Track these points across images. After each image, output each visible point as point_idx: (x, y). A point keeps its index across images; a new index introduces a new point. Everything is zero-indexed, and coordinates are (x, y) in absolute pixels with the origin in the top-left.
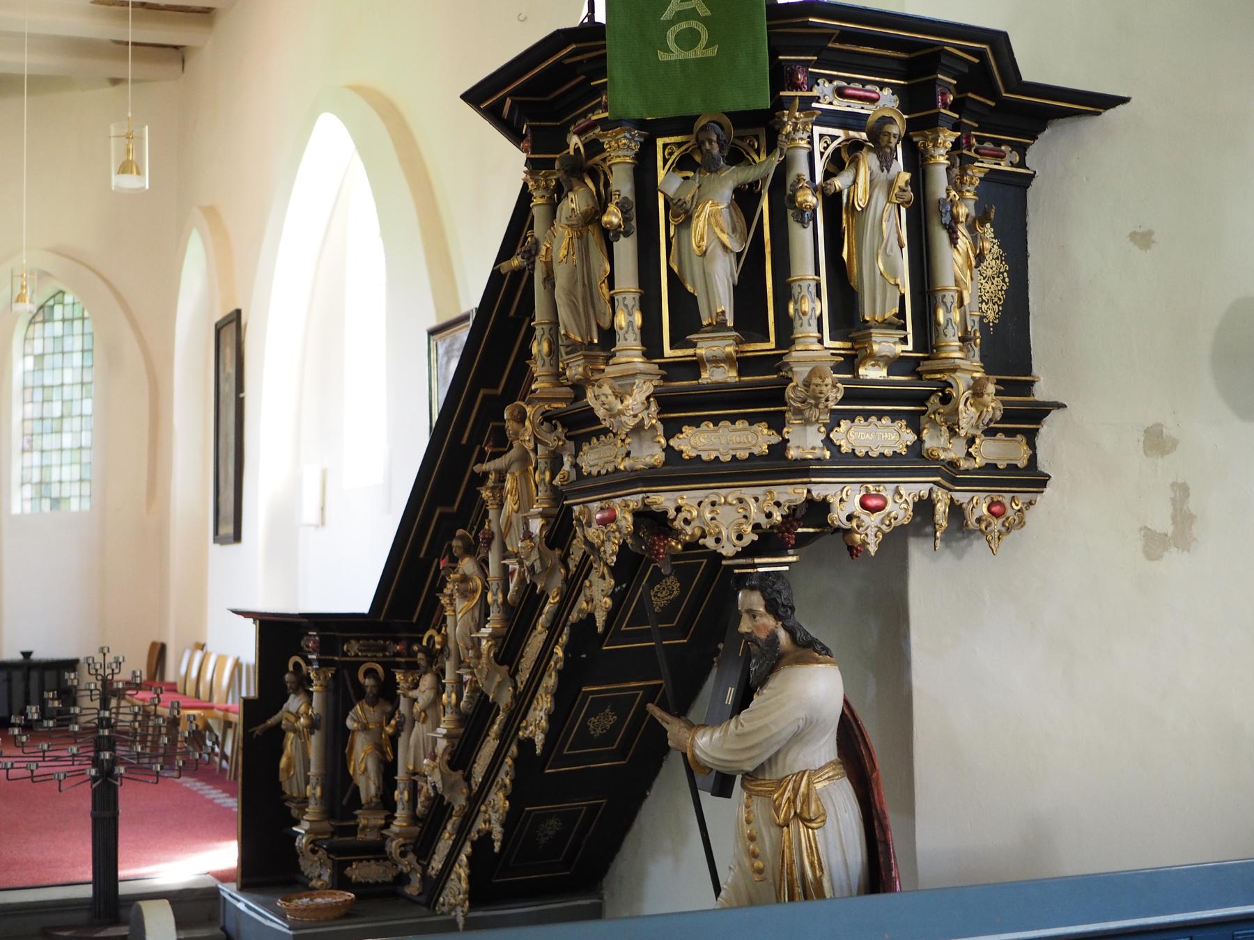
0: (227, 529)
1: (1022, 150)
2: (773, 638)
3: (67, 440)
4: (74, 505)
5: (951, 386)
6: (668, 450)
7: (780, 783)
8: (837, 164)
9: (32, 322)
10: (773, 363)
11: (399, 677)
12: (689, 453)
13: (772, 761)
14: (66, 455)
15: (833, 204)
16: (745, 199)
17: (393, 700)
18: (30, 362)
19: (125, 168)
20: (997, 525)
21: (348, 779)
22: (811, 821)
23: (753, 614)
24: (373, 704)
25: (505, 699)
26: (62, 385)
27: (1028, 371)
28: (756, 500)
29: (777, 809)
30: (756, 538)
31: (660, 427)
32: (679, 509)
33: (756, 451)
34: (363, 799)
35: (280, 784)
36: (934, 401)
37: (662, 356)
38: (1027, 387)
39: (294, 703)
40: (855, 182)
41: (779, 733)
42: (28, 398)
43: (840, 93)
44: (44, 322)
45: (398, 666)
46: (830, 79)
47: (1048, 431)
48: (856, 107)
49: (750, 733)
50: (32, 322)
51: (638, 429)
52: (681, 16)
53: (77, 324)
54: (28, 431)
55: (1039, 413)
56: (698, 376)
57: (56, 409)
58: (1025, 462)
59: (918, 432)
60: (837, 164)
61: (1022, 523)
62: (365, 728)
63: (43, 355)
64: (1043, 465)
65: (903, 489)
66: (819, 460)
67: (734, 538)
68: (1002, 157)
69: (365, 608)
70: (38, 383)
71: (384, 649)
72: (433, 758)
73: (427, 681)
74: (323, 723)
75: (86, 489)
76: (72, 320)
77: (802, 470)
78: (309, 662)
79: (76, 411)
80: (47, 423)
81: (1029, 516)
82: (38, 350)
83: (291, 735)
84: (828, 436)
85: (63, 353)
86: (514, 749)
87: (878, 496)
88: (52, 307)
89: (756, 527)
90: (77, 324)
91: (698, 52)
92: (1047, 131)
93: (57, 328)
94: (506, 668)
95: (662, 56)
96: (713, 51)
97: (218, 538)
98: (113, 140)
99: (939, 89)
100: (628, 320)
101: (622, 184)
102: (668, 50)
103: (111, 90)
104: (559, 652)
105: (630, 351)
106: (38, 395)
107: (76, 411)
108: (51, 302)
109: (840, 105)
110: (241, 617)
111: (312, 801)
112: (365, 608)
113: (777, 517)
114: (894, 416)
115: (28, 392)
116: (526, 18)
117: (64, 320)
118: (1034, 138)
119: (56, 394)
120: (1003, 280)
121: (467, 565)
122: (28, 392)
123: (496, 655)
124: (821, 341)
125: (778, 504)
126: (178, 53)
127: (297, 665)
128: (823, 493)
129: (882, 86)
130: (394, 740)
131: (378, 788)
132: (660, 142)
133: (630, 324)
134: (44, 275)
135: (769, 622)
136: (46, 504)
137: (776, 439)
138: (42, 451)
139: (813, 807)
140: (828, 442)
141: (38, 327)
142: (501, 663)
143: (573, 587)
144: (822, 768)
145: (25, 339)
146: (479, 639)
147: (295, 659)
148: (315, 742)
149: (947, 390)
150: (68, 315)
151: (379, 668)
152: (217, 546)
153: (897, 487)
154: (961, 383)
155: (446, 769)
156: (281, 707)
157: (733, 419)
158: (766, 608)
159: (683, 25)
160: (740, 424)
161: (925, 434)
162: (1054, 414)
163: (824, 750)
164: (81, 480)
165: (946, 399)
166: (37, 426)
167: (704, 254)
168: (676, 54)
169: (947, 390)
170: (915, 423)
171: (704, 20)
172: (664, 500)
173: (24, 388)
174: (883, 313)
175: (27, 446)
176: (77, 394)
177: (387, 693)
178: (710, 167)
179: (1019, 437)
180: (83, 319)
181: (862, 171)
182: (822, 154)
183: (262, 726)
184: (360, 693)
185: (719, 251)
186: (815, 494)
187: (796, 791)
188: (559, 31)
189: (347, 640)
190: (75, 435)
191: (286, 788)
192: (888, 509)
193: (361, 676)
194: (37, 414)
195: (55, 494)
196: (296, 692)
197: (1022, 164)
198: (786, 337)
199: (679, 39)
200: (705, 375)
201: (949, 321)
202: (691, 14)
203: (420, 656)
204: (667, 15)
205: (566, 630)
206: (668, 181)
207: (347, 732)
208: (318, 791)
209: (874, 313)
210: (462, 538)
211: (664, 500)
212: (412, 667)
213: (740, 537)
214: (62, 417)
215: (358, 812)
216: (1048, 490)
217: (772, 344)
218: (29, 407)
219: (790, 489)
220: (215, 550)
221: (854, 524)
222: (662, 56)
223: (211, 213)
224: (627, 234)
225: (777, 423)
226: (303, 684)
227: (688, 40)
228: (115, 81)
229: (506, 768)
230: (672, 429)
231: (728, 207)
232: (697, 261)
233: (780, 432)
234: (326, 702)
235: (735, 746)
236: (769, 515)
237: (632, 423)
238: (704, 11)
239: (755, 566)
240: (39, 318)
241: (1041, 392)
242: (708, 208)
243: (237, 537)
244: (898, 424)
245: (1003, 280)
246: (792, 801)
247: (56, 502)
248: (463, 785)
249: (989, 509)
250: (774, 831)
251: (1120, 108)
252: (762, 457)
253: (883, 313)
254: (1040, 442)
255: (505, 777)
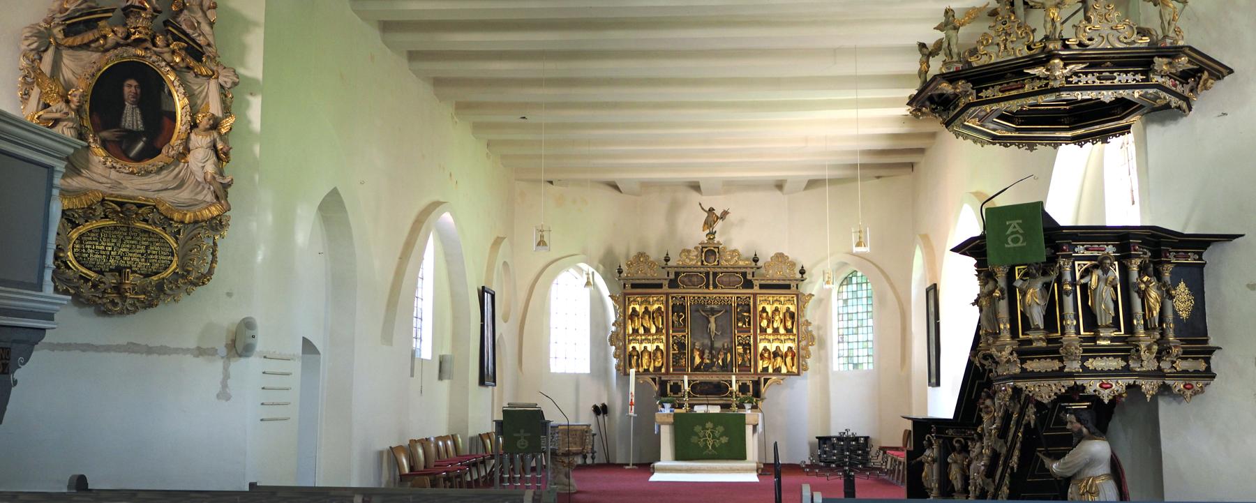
0: (934, 380)
1: (1200, 255)
2: (1080, 431)
3: (861, 338)
4: (865, 367)
5: (1138, 346)
6: (1022, 368)
7: (1082, 481)
8: (1087, 272)
9: (841, 285)
10: (1056, 340)
11: (969, 443)
12: (1029, 369)
13: (1079, 472)
14: (860, 344)
15: (1085, 288)
16: (1047, 286)
17: (968, 452)
18: (841, 302)
19: (859, 245)
20: (1189, 393)
21: (949, 482)
22: (1094, 493)
23: (1071, 422)
24: (959, 453)
25: (1004, 451)
26: (857, 313)
27: (1206, 335)
28: (1055, 385)
29: (1080, 489)
30: (1056, 397)
31: (1018, 361)
32: (1027, 387)
33: (1054, 369)
34: (956, 489)
35: (923, 483)
36: (1133, 351)
37: (1019, 338)
38: (1206, 341)
39: (928, 452)
40: (1091, 280)
41: (1079, 463)
42: (840, 319)
43: (1087, 249)
44: (847, 285)
45: (969, 439)
46: (1083, 245)
47: (1214, 358)
48: (1096, 253)
49: (1068, 463)
50: (841, 285)
51: (1008, 361)
52: (1012, 233)
53: (864, 285)
54: (841, 333)
55: (1211, 351)
56: (1032, 344)
57: (854, 324)
58: (1204, 369)
59: (1127, 362)
60: (1087, 272)
61: (1203, 391)
62: (955, 462)
63: (848, 299)
64: (1214, 369)
65: (1120, 382)
66: (1078, 372)
67: (1047, 397)
68: (1189, 257)
69: (951, 417)
70: (845, 311)
71: (965, 433)
72: (978, 473)
73: (978, 444)
74: (938, 460)
75: (871, 360)
76: (862, 284)
77: (1070, 375)
78: (932, 436)
79: (865, 324)
80: (850, 330)
81: (1207, 389)
82: (845, 297)
83: (927, 464)
84: (1083, 364)
85: (857, 298)
86: (1009, 470)
87: (1108, 383)
88: (851, 278)
89: (1056, 394)
90: (864, 285)
91: (1019, 244)
92: (1211, 247)
93: (854, 287)
94: (1003, 440)
95: (1006, 246)
96: (1025, 244)
97: (930, 384)
98: (853, 234)
99: (1132, 245)
100: (1005, 326)
101: (1002, 283)
102: (1008, 244)
103: (877, 180)
104: (1020, 435)
105: (1006, 337)
106: (845, 317)
107: (865, 324)
108: (851, 276)
109: (1088, 253)
110: (906, 420)
111: (934, 489)
112: (951, 417)
113: (1063, 391)
114: (1115, 357)
115: (841, 316)
116: (1038, 178)
117: (857, 284)
118: (1206, 249)
119: (855, 316)
120: (1191, 302)
121: (988, 402)
122: (841, 316)
123: (998, 435)
124: (1078, 332)
125: (1063, 386)
126: (912, 165)
127: (929, 438)
128: (1081, 383)
129: (1107, 245)
130: (968, 466)
131: (962, 485)
132: (1017, 268)
133: (1005, 328)
134: (844, 264)
135: (1078, 425)
136: (851, 366)
137: (1061, 365)
138: (848, 342)
139: (1094, 489)
140: (1083, 366)
141: (845, 287)
142: (1001, 438)
143: (1022, 414)
144: (1099, 476)
145: (838, 292)
146: (991, 430)
147: (928, 435)
148: (935, 466)
149: (1137, 348)
150: (859, 281)
151: (962, 440)
152: (930, 387)
153: (576, 422)
154: (1143, 346)
155: (984, 478)
156: (923, 454)
157: (1045, 358)
158: (1077, 420)
159: (1014, 236)
160: (1048, 360)
161: (1130, 362)
162: (1217, 351)
163: (1104, 469)
164: (868, 356)
165: (1138, 351)
166: (845, 332)
167: (1030, 306)
168: (1012, 245)
169: (1137, 348)
170: (1125, 359)
171: (1021, 234)
172: (1020, 384)
173: (839, 314)
174: (1106, 322)
175: (841, 340)
176: (865, 317)
177: (965, 449)
178: (1033, 277)
179: (1200, 360)
180: (867, 283)
181: (1094, 276)
182: (1079, 271)
183: (915, 461)
184: (954, 449)
185: (1035, 305)
186: (1078, 383)
187: (1087, 483)
188: (972, 238)
189: (947, 429)
190: (866, 334)
191: (925, 484)
192: (1113, 388)
193: (954, 443)
194: (846, 326)
195: (855, 362)
196: (929, 448)
197: (1200, 259)
198: (1063, 333)
199: (1012, 240)
200: (1034, 344)
201: (1138, 324)
202: (1017, 232)
203: (975, 435)
204: (1008, 232)
205: (1022, 427)
206: (1018, 283)
207: (948, 464)
208: (937, 485)
209: (1102, 322)
210: (986, 392)
211: (1020, 384)
212: (973, 440)
213: (1050, 397)
214: (858, 327)
215: (954, 494)
216: (1215, 380)
217: (1123, 332)
218: (841, 323)
219: (1067, 381)
220: (930, 388)
221: (1097, 393)
222: (1006, 246)
223: (926, 238)
224: (1003, 299)
225: (1061, 360)
226: (930, 445)
227: (1015, 240)
228: (878, 177)
229: (1006, 478)
230: (1023, 361)
231: (1040, 290)
232: (1028, 308)
233: (1063, 363)
234: (940, 451)
235: (1064, 467)
236: (1060, 390)
237: (1005, 360)
238: (1021, 231)
239: (1071, 406)
240: (845, 283)
241: (1212, 342)
242: (1031, 291)
243: (938, 384)
244: (1117, 359)
245: (1191, 302)
246: (1085, 487)
247: (856, 366)
248: (992, 483)
249: (1184, 386)
250: (1080, 497)
251: (1240, 238)
252: (1056, 371)
253: (1106, 322)
254: (1212, 362)
255: (1007, 481)
